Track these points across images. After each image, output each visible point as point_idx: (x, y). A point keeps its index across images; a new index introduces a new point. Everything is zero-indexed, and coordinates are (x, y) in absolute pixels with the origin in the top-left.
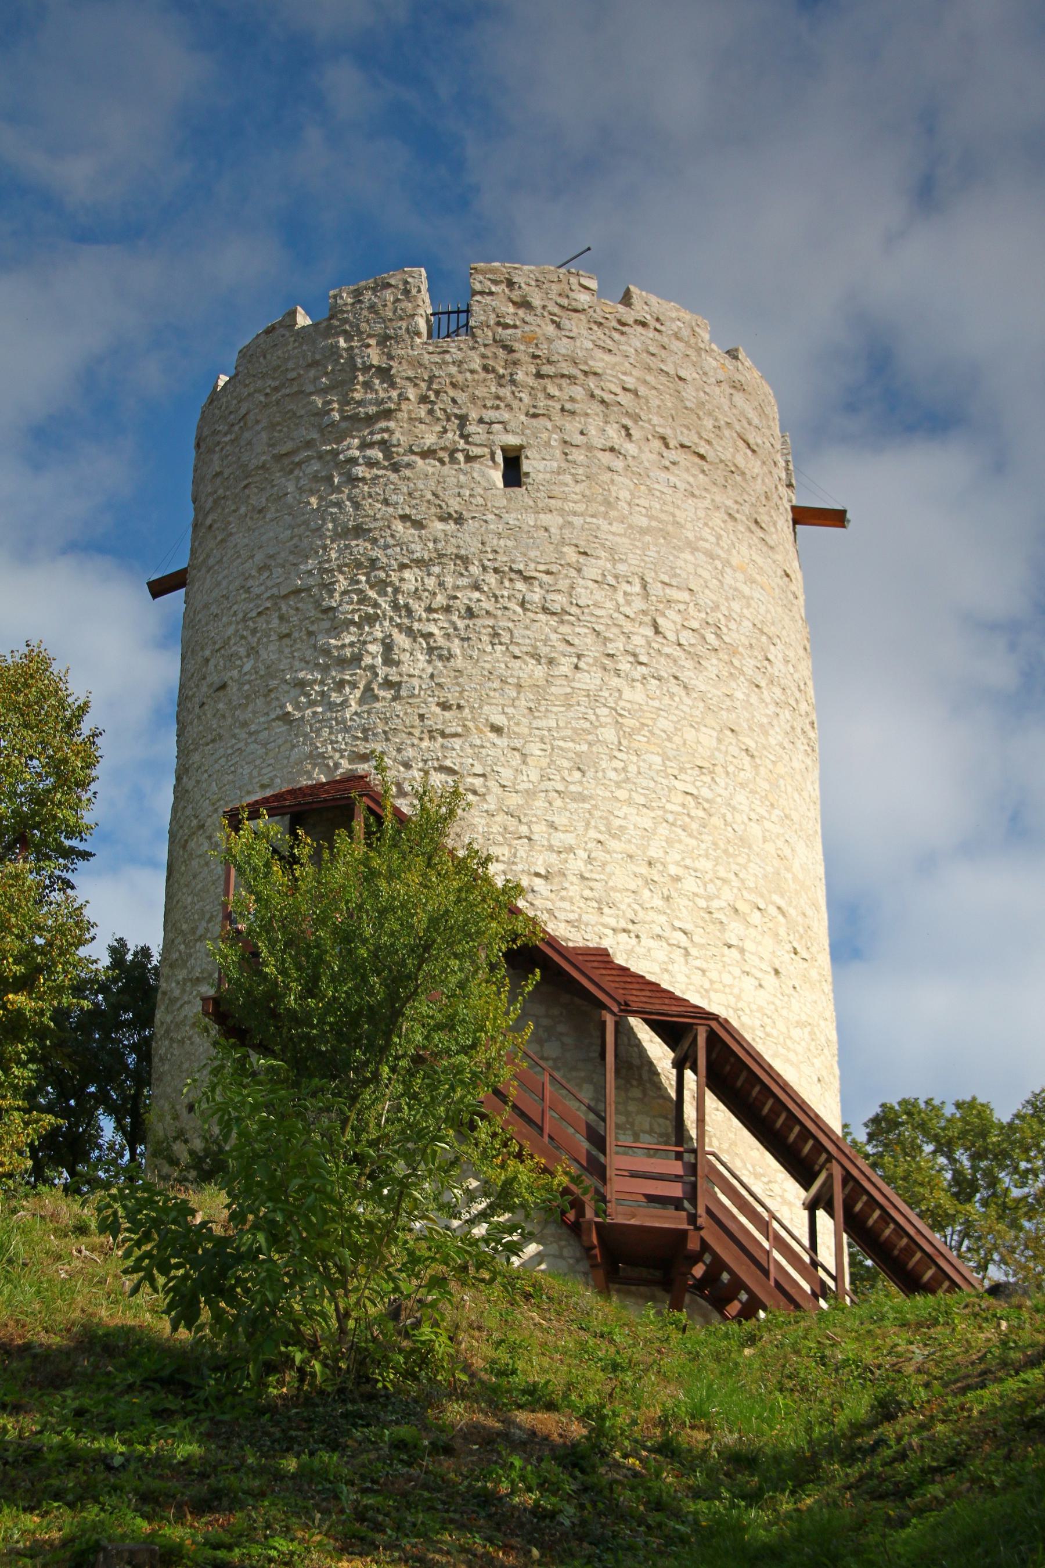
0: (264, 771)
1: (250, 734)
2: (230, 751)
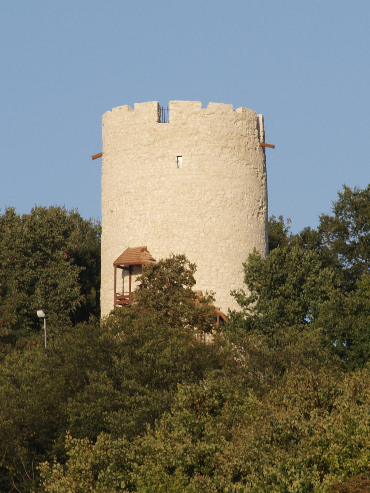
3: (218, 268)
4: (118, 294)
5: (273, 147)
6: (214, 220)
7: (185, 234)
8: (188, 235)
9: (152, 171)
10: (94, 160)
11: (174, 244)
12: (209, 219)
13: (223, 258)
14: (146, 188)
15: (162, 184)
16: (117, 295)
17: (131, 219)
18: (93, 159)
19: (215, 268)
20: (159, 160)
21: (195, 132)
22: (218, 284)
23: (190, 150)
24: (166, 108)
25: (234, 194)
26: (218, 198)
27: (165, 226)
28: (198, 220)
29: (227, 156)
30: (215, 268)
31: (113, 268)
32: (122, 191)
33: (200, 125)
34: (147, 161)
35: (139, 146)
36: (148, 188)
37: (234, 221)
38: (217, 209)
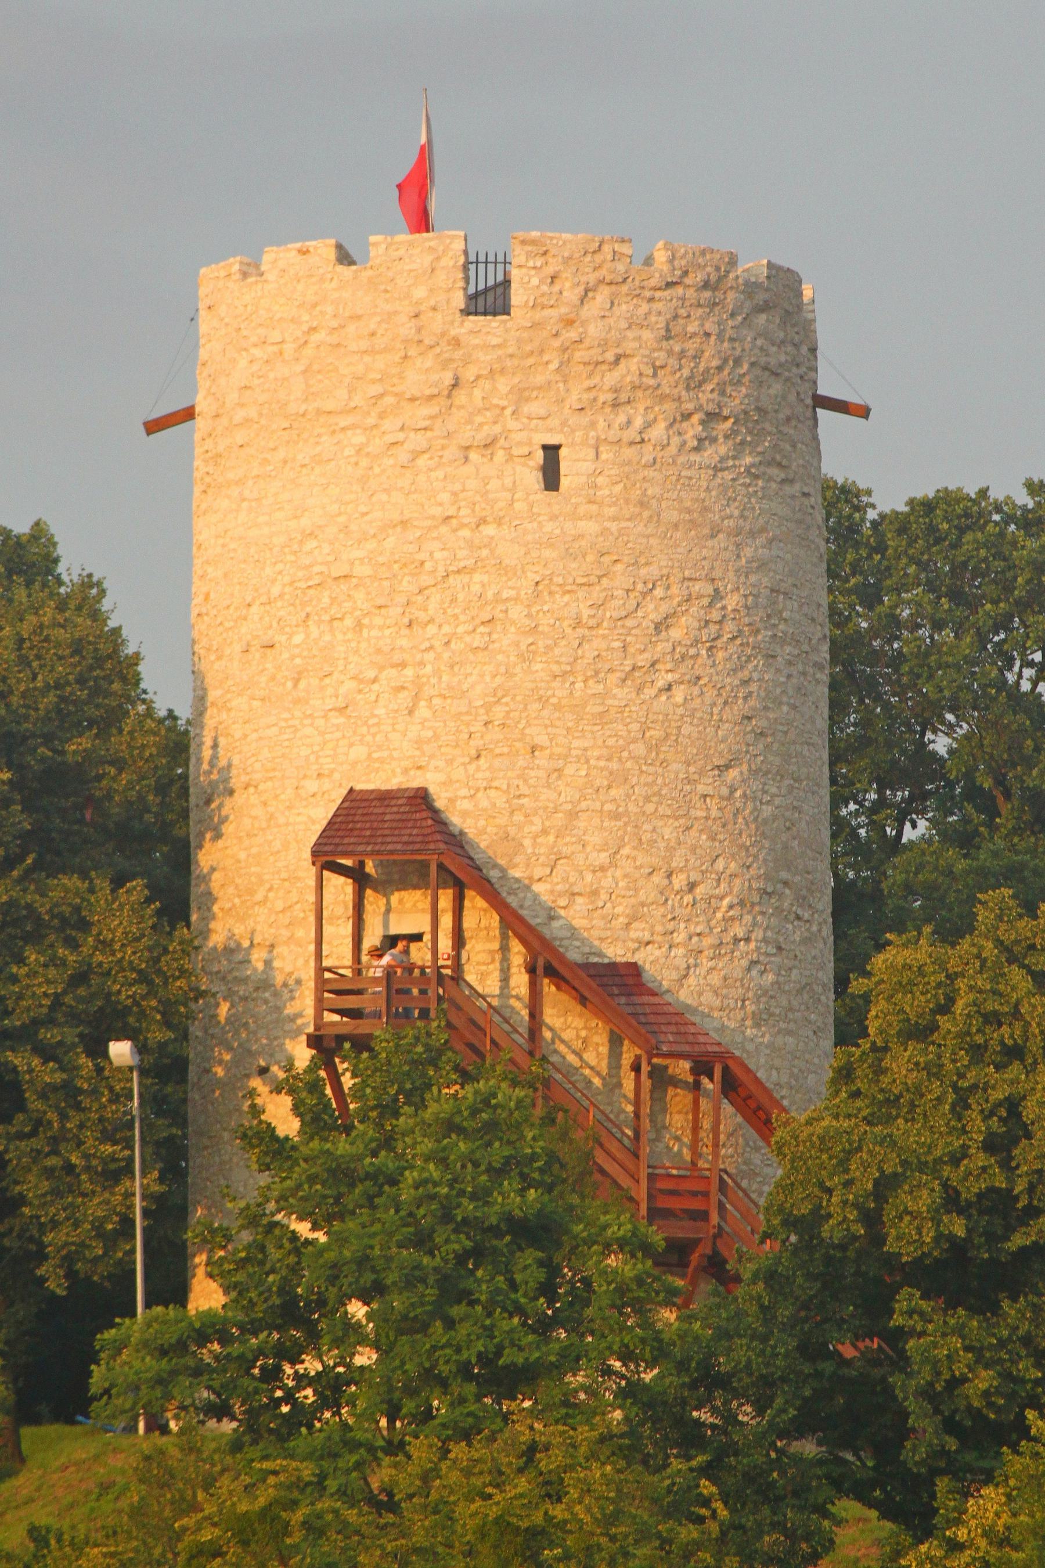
0: (322, 760)
1: (307, 717)
2: (283, 724)
3: (694, 876)
4: (329, 970)
5: (863, 412)
6: (679, 694)
7: (576, 743)
8: (585, 750)
9: (445, 497)
10: (152, 436)
11: (532, 782)
12: (660, 691)
13: (713, 839)
14: (422, 563)
15: (485, 552)
16: (327, 975)
17: (361, 681)
18: (148, 434)
19: (683, 876)
20: (473, 456)
21: (610, 356)
22: (695, 939)
23: (593, 424)
24: (501, 258)
25: (745, 596)
26: (693, 610)
27: (499, 712)
28: (623, 693)
29: (723, 450)
30: (683, 876)
31: (309, 873)
32: (317, 569)
33: (629, 327)
34: (422, 462)
35: (389, 400)
36: (428, 566)
37: (745, 698)
38: (692, 651)
